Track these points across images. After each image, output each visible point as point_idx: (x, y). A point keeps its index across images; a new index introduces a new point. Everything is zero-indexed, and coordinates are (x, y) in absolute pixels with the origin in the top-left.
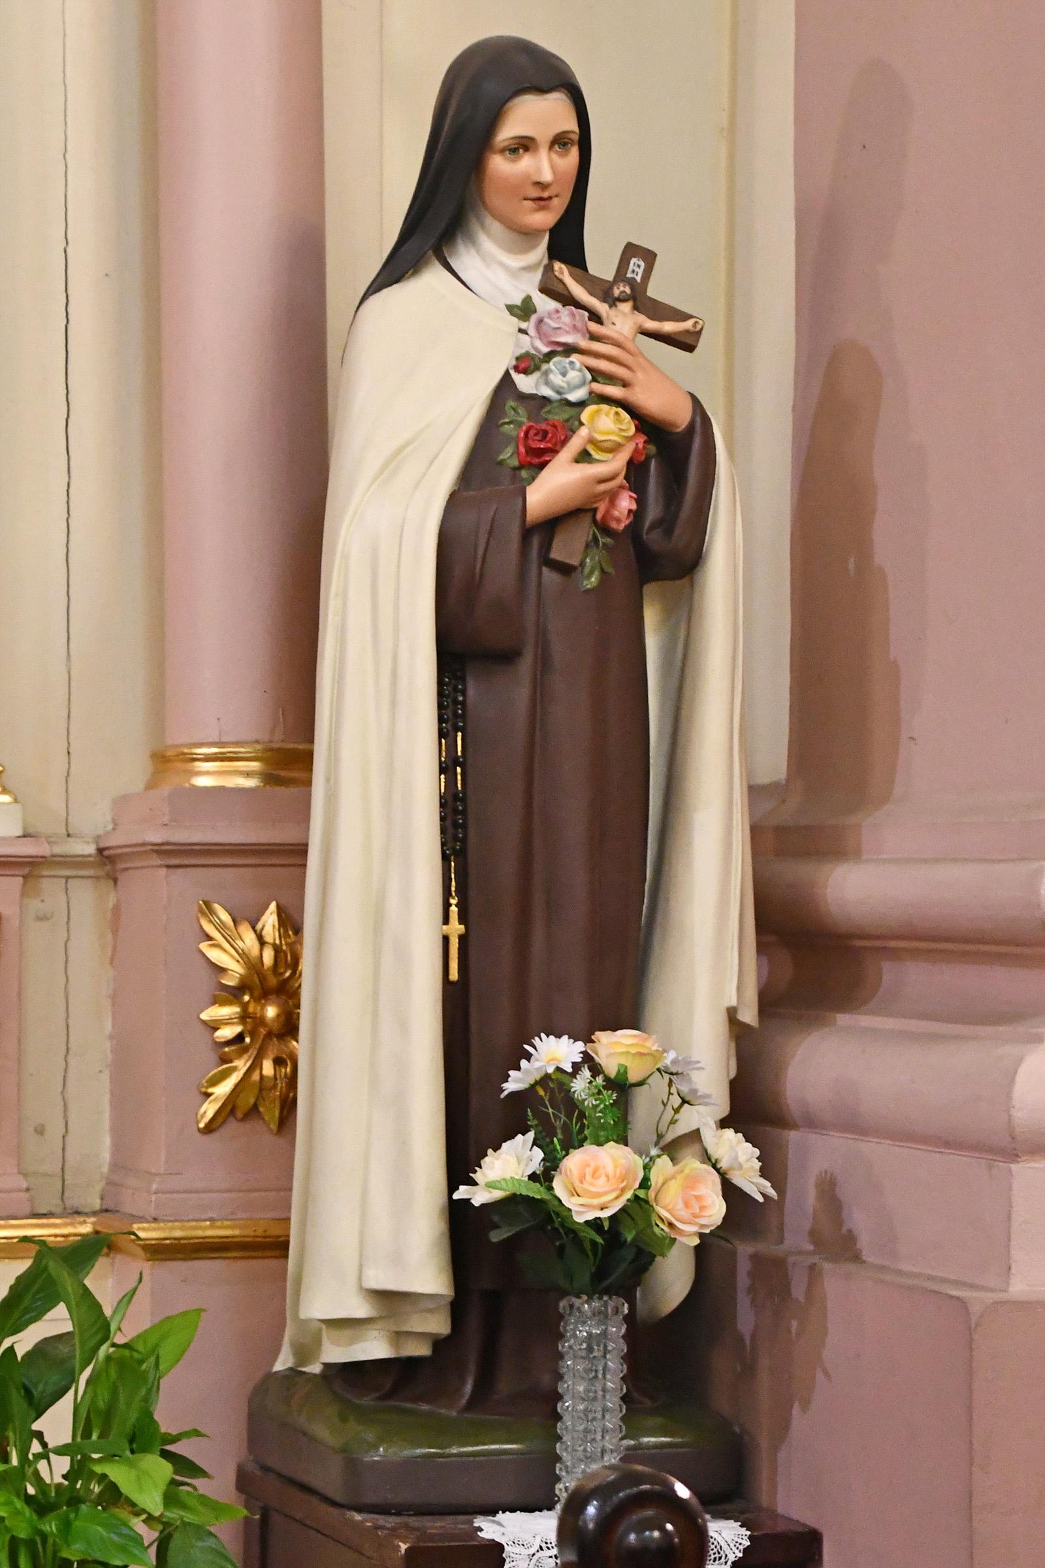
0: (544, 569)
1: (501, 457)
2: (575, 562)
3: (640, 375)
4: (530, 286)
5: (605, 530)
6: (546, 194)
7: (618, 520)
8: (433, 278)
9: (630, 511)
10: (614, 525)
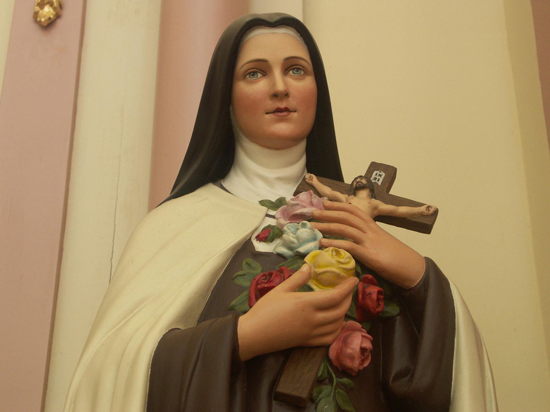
0: (274, 402)
1: (233, 303)
2: (304, 394)
3: (370, 234)
4: (286, 192)
5: (344, 372)
6: (283, 105)
7: (352, 358)
8: (208, 194)
9: (363, 350)
10: (348, 363)
